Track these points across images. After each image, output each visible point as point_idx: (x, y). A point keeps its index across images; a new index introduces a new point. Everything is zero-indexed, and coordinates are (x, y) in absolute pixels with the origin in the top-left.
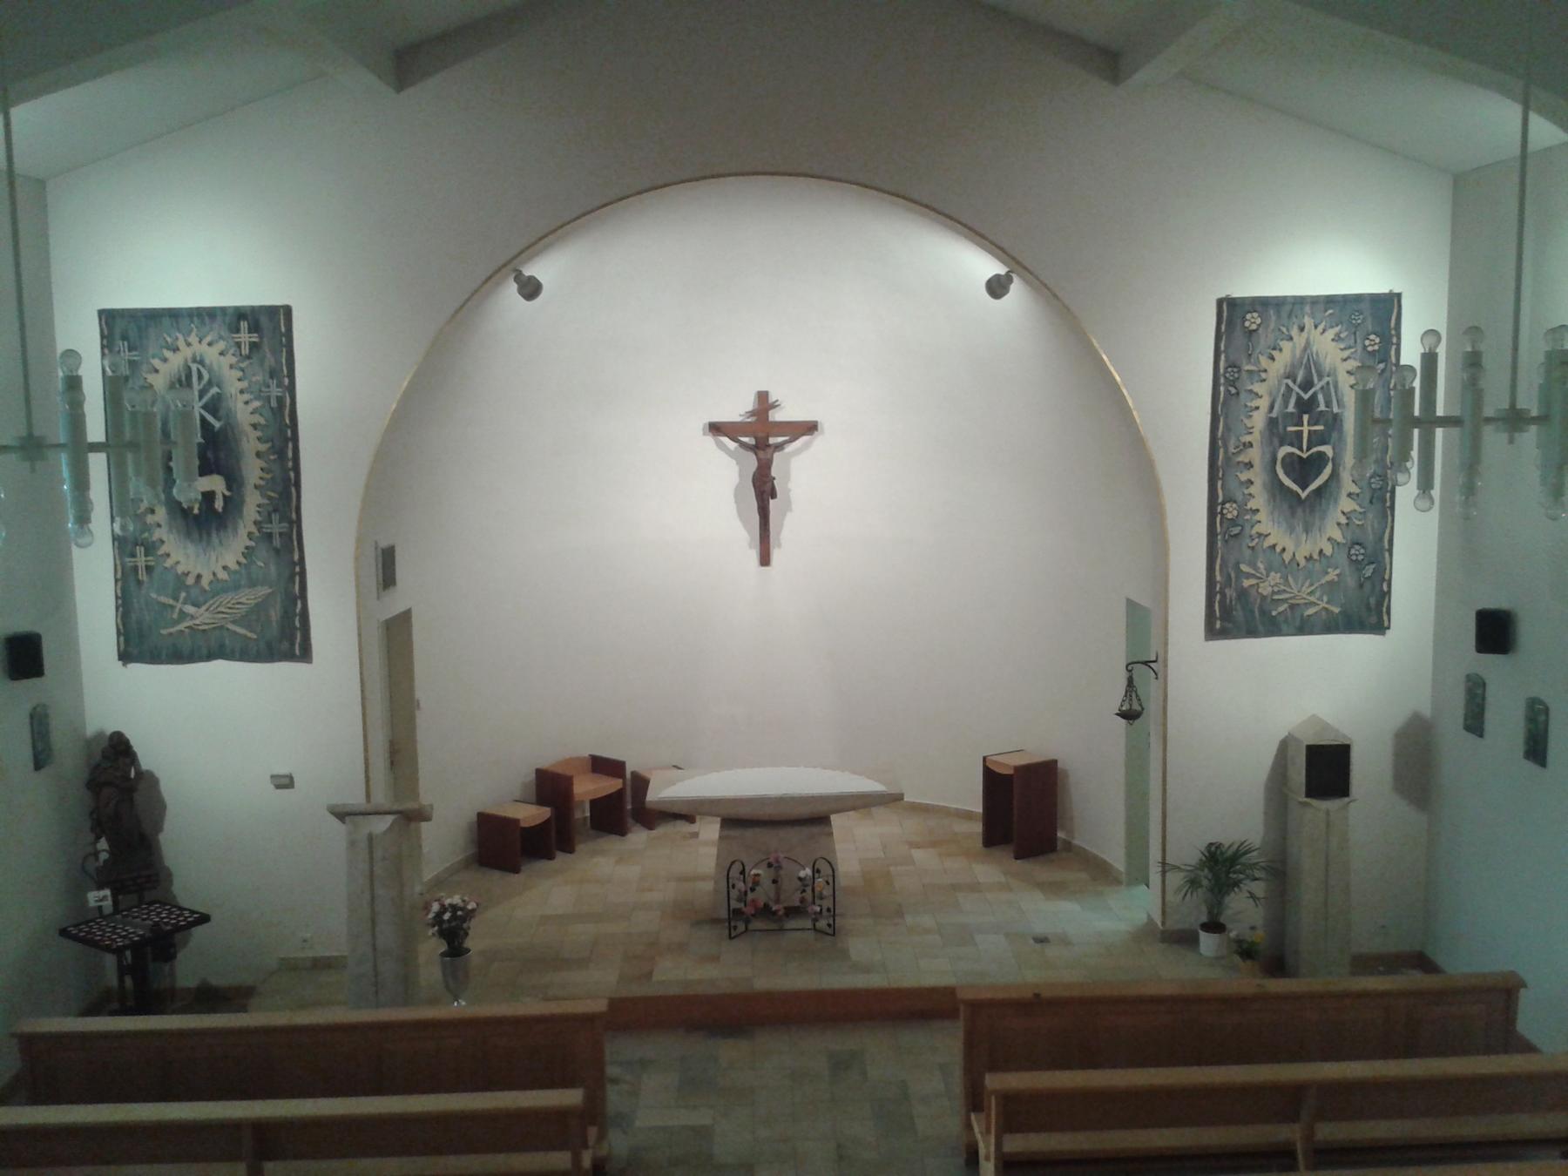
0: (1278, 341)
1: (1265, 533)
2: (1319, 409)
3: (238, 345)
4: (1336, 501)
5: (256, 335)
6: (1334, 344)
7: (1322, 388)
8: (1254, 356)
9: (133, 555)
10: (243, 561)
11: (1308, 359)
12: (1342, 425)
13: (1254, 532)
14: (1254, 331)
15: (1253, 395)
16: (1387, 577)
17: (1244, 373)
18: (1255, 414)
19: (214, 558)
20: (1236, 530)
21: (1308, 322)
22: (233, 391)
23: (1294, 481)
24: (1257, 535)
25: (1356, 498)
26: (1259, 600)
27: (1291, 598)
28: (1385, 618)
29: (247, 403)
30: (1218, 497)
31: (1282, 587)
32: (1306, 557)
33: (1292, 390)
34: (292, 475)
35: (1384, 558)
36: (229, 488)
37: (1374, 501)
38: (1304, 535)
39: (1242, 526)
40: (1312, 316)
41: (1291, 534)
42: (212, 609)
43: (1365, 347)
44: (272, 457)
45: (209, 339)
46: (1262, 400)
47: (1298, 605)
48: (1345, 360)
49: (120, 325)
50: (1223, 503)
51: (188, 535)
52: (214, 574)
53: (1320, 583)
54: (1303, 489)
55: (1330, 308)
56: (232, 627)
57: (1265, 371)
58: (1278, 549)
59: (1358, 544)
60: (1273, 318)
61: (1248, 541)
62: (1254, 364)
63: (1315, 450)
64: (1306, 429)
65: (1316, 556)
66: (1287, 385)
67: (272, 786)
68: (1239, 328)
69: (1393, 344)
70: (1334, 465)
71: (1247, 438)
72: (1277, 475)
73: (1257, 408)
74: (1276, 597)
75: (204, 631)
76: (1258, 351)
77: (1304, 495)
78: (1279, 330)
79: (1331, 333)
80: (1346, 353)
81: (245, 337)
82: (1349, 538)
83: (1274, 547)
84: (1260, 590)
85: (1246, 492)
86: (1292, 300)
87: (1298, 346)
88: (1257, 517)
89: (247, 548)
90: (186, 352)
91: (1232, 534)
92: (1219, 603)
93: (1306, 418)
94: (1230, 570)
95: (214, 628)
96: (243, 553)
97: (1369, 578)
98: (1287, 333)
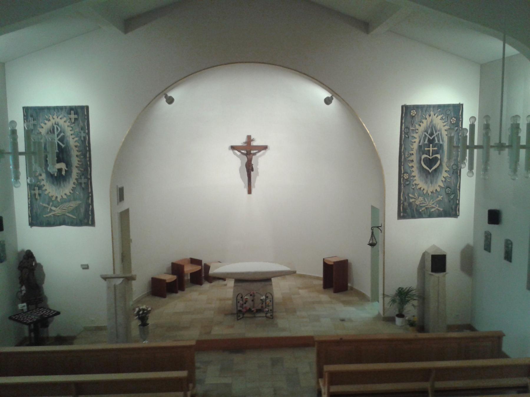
1: (417, 184)
3: (70, 119)
4: (441, 173)
6: (441, 120)
7: (437, 135)
9: (34, 190)
10: (72, 192)
11: (432, 126)
13: (414, 183)
14: (414, 116)
16: (458, 198)
18: (414, 144)
19: (61, 191)
20: (407, 183)
21: (432, 113)
26: (415, 206)
28: (458, 212)
29: (73, 139)
31: (423, 202)
36: (67, 167)
37: (454, 173)
38: (431, 185)
43: (451, 122)
44: (82, 157)
47: (428, 208)
48: (445, 126)
49: (30, 112)
50: (404, 173)
51: (53, 183)
52: (62, 196)
56: (68, 214)
57: (418, 130)
61: (412, 186)
62: (414, 127)
64: (431, 149)
65: (434, 192)
66: (425, 135)
71: (412, 152)
73: (415, 142)
74: (421, 205)
77: (430, 171)
78: (422, 116)
79: (440, 117)
80: (445, 124)
81: (73, 116)
83: (420, 188)
84: (416, 203)
87: (428, 121)
88: (415, 178)
89: (73, 188)
90: (53, 121)
92: (91, 221)
93: (431, 145)
96: (72, 190)
97: (452, 199)
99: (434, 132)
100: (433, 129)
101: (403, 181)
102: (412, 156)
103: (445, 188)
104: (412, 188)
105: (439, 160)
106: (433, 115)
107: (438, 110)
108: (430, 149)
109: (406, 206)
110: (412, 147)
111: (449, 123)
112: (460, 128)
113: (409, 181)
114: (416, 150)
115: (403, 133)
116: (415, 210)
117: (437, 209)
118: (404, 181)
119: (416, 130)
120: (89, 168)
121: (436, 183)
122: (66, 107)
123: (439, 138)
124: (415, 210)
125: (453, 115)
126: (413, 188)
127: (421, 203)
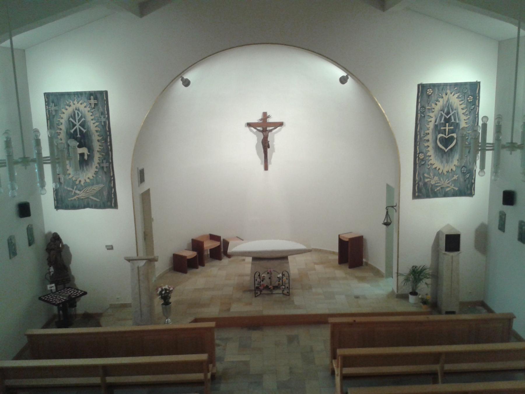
1: (433, 163)
2: (452, 121)
5: (96, 101)
6: (457, 99)
7: (453, 114)
10: (94, 176)
11: (448, 105)
13: (429, 163)
20: (423, 163)
21: (449, 92)
22: (89, 120)
28: (473, 191)
29: (94, 123)
30: (417, 152)
31: (439, 182)
34: (109, 147)
36: (89, 152)
40: (450, 89)
42: (84, 192)
43: (468, 100)
45: (81, 102)
48: (461, 105)
49: (51, 98)
50: (419, 153)
52: (85, 180)
54: (446, 148)
56: (91, 197)
57: (434, 109)
58: (437, 169)
61: (427, 166)
64: (447, 128)
65: (450, 171)
66: (441, 113)
67: (106, 249)
70: (457, 140)
71: (428, 132)
74: (437, 185)
75: (82, 199)
77: (446, 151)
78: (439, 95)
79: (456, 96)
80: (461, 102)
81: (93, 101)
84: (431, 182)
88: (430, 158)
89: (96, 171)
90: (73, 107)
91: (422, 164)
93: (447, 124)
95: (86, 198)
99: (451, 111)
106: (449, 95)
108: (446, 128)
111: (466, 100)
115: (419, 112)
118: (420, 161)
120: (110, 152)
122: (85, 92)
125: (470, 93)
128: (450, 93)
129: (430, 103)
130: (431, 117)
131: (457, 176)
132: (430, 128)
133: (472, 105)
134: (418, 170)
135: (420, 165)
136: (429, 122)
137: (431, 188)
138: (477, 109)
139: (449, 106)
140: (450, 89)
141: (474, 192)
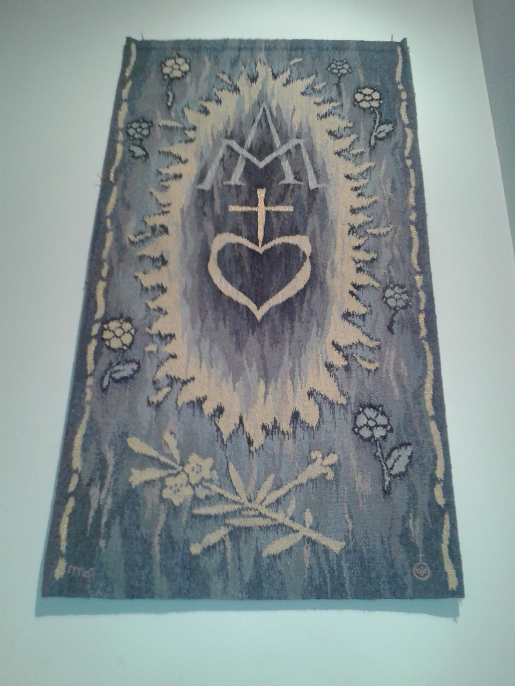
0: (215, 90)
1: (183, 377)
2: (285, 182)
4: (321, 325)
6: (306, 98)
7: (288, 152)
8: (177, 107)
11: (265, 115)
12: (325, 207)
13: (161, 375)
14: (178, 78)
15: (171, 158)
16: (440, 474)
17: (158, 129)
18: (174, 184)
20: (127, 370)
21: (263, 71)
23: (241, 289)
24: (167, 382)
25: (361, 323)
26: (163, 517)
27: (233, 514)
28: (449, 567)
30: (95, 312)
31: (216, 489)
32: (264, 427)
33: (237, 155)
35: (430, 436)
37: (395, 327)
38: (262, 383)
39: (138, 363)
40: (269, 62)
41: (234, 382)
43: (355, 103)
46: (188, 166)
47: (248, 529)
48: (325, 116)
50: (105, 320)
53: (296, 482)
54: (259, 304)
55: (297, 56)
57: (194, 128)
58: (209, 408)
59: (370, 406)
60: (208, 65)
61: (150, 390)
62: (177, 119)
63: (278, 241)
64: (261, 210)
65: (285, 425)
66: (229, 148)
68: (153, 75)
69: (401, 101)
70: (314, 266)
71: (160, 220)
72: (210, 279)
73: (178, 177)
74: (203, 511)
76: (185, 102)
77: (259, 314)
78: (218, 77)
79: (300, 85)
80: (325, 108)
82: (352, 394)
83: (200, 402)
84: (167, 494)
85: (152, 305)
86: (237, 45)
87: (246, 99)
88: (169, 348)
91: (117, 376)
92: (71, 516)
93: (261, 193)
94: (106, 447)
97: (401, 475)
98: (231, 83)
99: (277, 141)
100: (272, 126)
101: (96, 361)
102: (163, 239)
103: (353, 408)
104: (149, 404)
105: (308, 260)
106: (266, 79)
107: (291, 58)
108: (255, 209)
109: (99, 512)
110: (163, 200)
111: (347, 105)
112: (404, 126)
113: (132, 361)
114: (182, 211)
115: (121, 137)
116: (156, 548)
117: (309, 540)
118: (104, 361)
119: (184, 129)
121: (293, 378)
123: (303, 163)
124: (156, 548)
125: (362, 79)
126: (154, 399)
127: (201, 493)
128: (271, 77)
129: (174, 109)
130: (180, 158)
131: (332, 459)
132: (171, 208)
133: (381, 123)
134: (88, 409)
135: (105, 383)
136: (167, 180)
137: (167, 529)
138: (405, 136)
139: (266, 121)
140: (268, 60)
141: (459, 574)
